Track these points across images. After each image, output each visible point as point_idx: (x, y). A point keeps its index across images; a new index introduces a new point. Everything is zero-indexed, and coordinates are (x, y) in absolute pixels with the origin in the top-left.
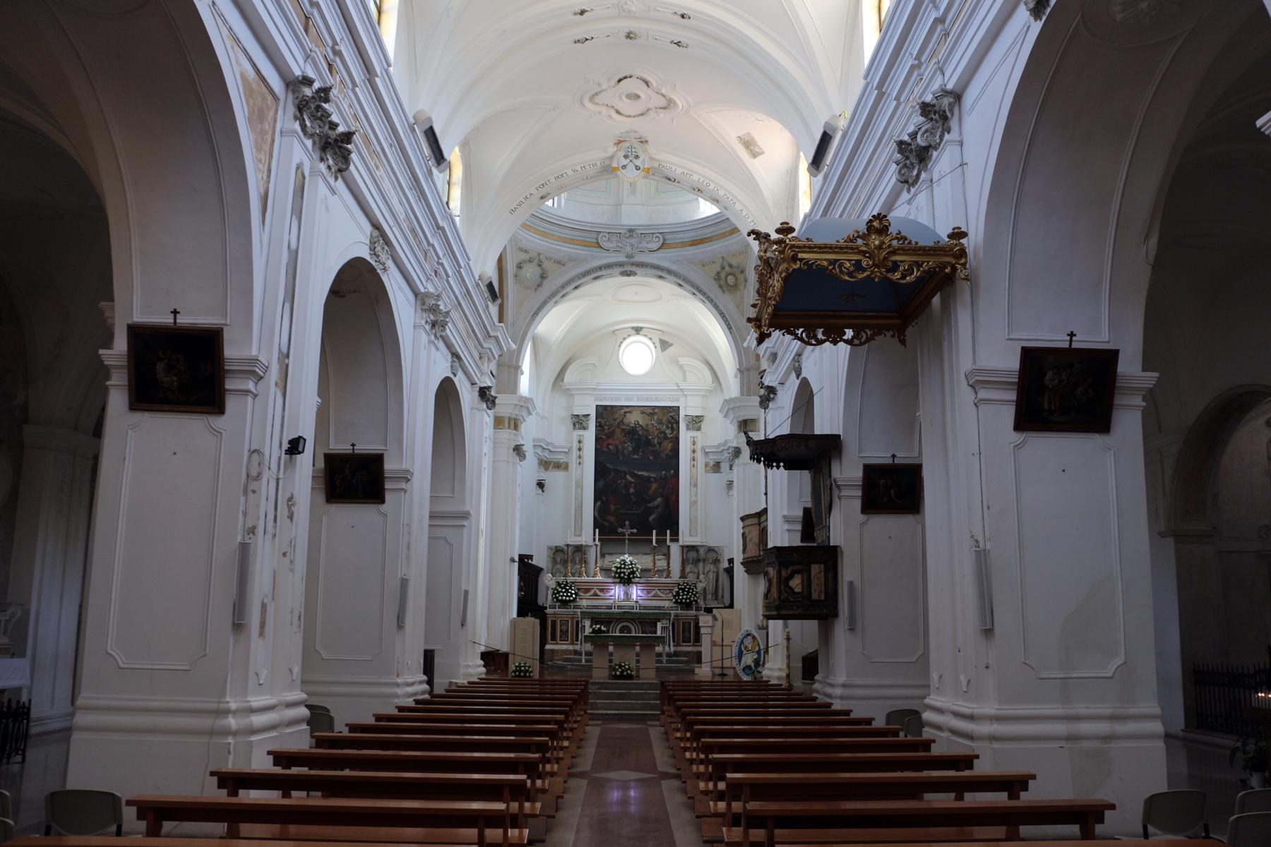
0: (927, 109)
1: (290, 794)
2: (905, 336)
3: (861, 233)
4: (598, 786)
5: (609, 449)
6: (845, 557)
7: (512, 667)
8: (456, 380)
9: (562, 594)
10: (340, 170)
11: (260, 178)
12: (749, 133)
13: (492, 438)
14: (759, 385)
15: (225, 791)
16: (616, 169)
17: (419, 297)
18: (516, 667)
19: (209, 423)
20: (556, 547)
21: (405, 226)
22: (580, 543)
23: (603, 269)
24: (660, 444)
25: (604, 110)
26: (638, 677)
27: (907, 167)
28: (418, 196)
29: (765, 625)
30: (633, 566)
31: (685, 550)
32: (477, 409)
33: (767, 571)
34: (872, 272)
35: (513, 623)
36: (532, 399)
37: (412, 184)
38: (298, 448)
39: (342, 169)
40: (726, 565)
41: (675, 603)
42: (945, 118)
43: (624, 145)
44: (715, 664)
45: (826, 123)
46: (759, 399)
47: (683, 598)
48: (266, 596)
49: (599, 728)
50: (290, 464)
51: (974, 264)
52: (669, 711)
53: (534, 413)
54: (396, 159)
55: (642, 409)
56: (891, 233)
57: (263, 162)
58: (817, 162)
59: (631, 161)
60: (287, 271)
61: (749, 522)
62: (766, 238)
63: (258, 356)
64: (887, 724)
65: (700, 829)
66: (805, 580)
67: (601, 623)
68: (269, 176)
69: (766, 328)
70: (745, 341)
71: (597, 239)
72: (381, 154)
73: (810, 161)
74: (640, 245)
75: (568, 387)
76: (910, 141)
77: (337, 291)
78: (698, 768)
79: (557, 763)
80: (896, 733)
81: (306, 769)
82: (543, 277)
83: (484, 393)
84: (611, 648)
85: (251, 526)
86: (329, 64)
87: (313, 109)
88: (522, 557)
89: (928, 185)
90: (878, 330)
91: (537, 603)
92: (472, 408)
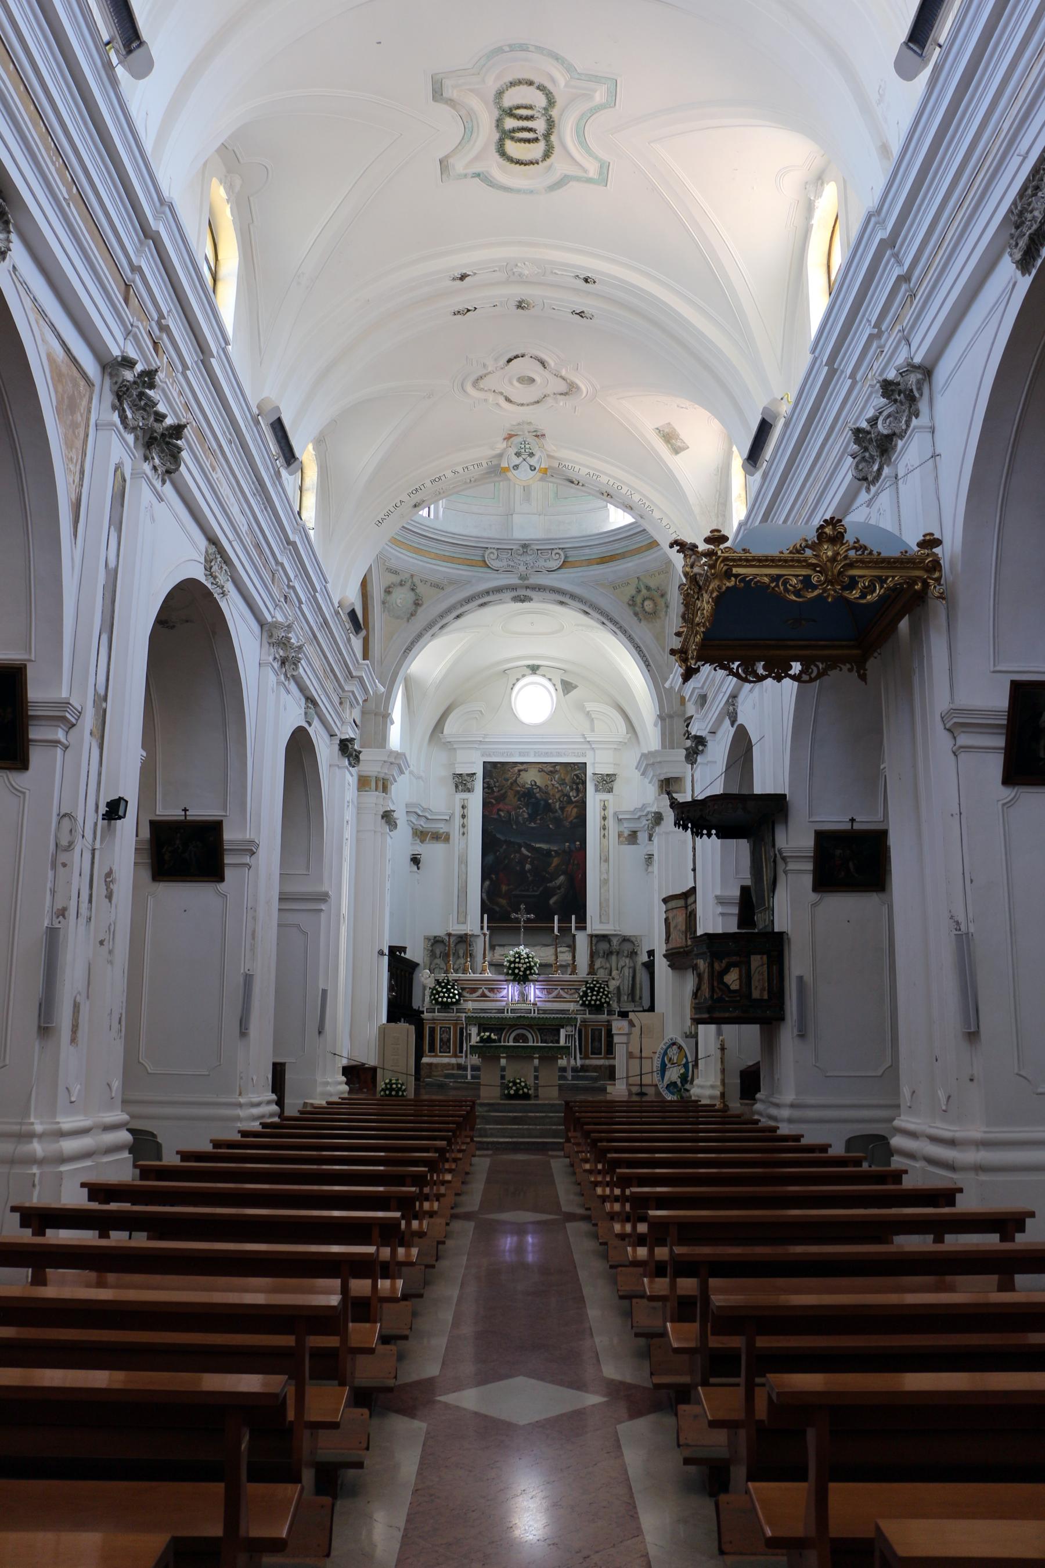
0: (890, 389)
1: (109, 1234)
2: (866, 670)
3: (810, 542)
4: (488, 1231)
5: (500, 816)
6: (793, 947)
7: (380, 1085)
8: (311, 730)
9: (442, 994)
10: (168, 472)
11: (71, 481)
12: (669, 423)
13: (356, 803)
14: (684, 735)
15: (28, 1232)
16: (507, 469)
17: (266, 628)
18: (386, 1084)
19: (8, 779)
20: (435, 937)
21: (248, 541)
22: (465, 932)
23: (491, 593)
24: (562, 809)
25: (491, 397)
26: (537, 1097)
27: (866, 461)
28: (263, 504)
29: (693, 1033)
30: (531, 959)
31: (594, 940)
32: (338, 766)
33: (696, 964)
34: (825, 590)
35: (382, 1030)
36: (404, 755)
37: (256, 489)
38: (118, 811)
39: (170, 471)
40: (645, 958)
41: (582, 1005)
42: (912, 399)
43: (516, 440)
44: (631, 1080)
45: (765, 409)
46: (684, 752)
47: (592, 1000)
48: (79, 993)
49: (488, 1160)
50: (109, 831)
51: (950, 579)
52: (575, 1137)
53: (407, 772)
54: (236, 458)
55: (541, 767)
56: (847, 541)
57: (75, 461)
58: (753, 457)
59: (524, 460)
60: (103, 610)
61: (673, 904)
62: (692, 550)
63: (69, 699)
64: (847, 1150)
65: (614, 1281)
66: (744, 975)
67: (491, 1030)
68: (82, 479)
69: (693, 662)
70: (666, 680)
71: (483, 556)
72: (218, 451)
73: (746, 455)
74: (537, 565)
75: (448, 740)
76: (868, 428)
77: (164, 621)
78: (612, 1207)
79: (438, 1200)
80: (858, 1163)
81: (129, 1204)
82: (417, 604)
83: (345, 746)
84: (503, 1062)
85: (60, 907)
86: (154, 342)
87: (135, 396)
88: (393, 950)
89: (893, 482)
90: (833, 663)
91: (412, 1007)
92: (330, 766)
